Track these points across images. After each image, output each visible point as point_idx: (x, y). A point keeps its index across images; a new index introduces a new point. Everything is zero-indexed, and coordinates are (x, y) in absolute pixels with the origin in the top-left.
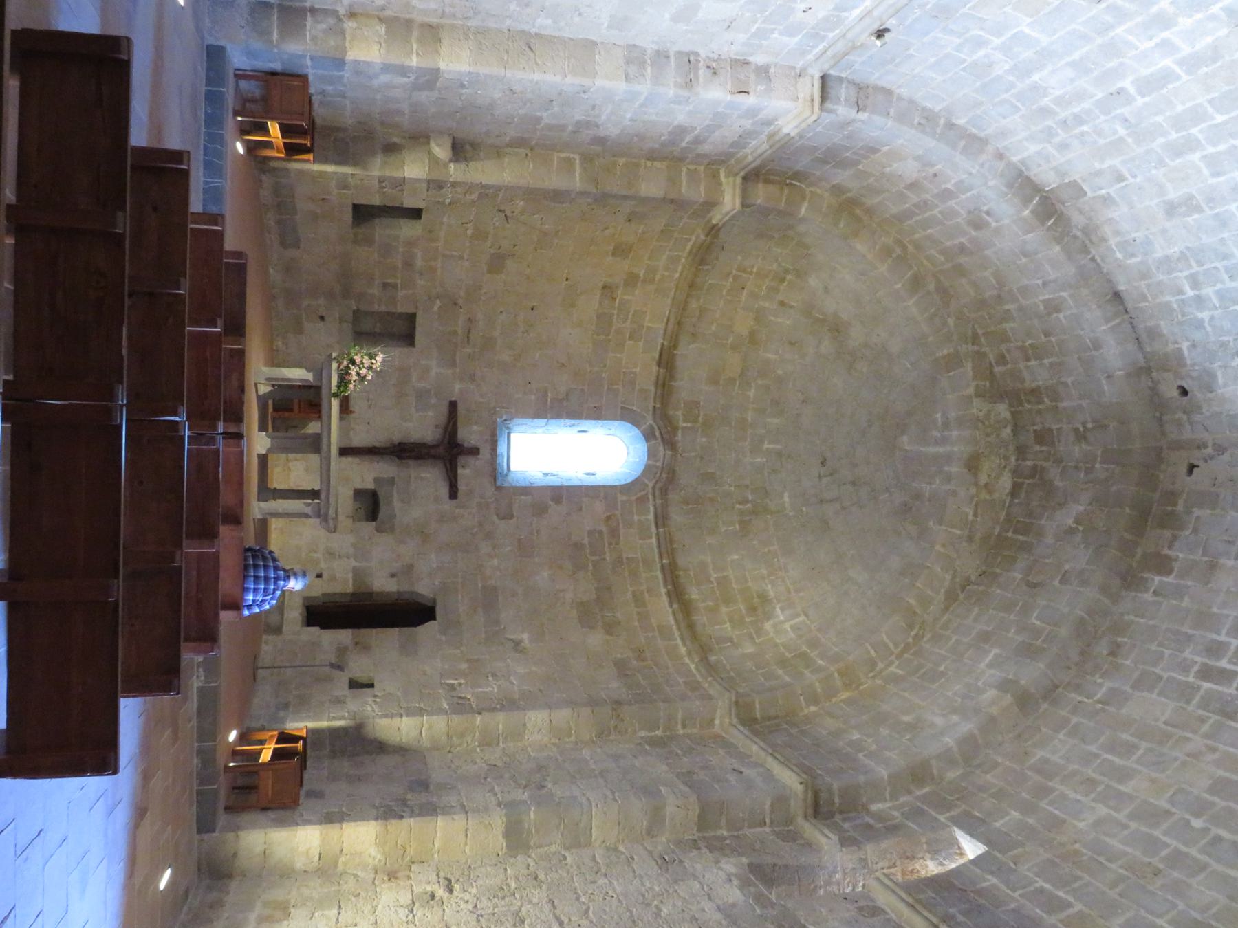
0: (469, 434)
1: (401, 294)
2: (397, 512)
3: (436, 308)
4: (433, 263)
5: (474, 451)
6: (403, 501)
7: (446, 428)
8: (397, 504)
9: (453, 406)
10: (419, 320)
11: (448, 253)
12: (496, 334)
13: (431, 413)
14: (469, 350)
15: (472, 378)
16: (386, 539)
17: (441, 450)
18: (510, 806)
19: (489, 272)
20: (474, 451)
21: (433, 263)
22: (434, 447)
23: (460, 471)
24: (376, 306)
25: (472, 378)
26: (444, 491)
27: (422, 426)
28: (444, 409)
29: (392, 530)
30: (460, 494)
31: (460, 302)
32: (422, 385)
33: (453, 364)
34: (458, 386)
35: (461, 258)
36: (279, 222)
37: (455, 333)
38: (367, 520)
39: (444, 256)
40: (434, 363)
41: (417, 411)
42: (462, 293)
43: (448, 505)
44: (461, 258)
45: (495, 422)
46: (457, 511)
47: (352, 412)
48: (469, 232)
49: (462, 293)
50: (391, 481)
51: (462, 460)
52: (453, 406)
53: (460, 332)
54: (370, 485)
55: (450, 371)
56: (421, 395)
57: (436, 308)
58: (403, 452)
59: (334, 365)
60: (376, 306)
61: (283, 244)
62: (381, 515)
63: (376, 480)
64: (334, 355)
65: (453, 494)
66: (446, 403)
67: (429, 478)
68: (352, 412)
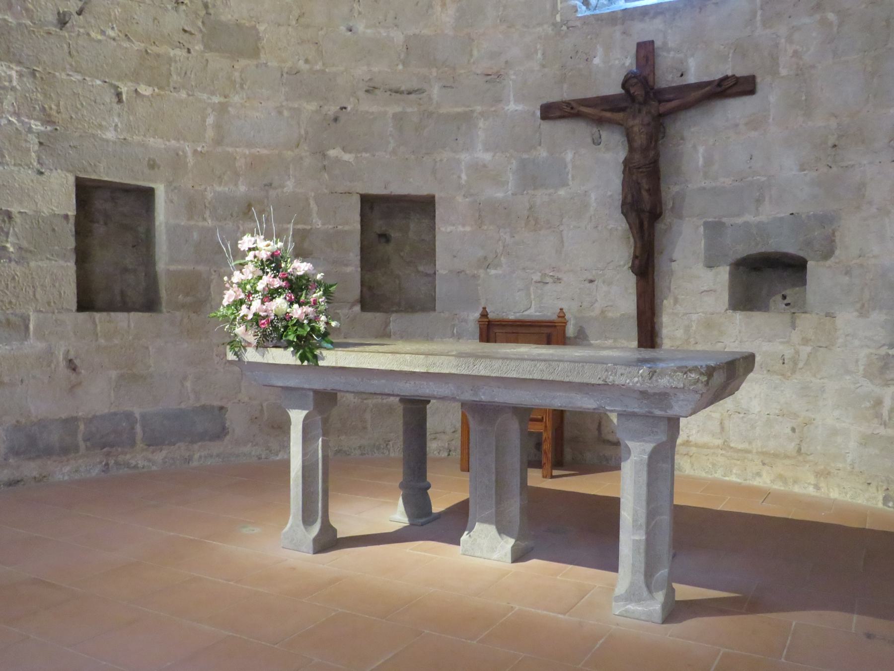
0: (607, 70)
1: (318, 223)
2: (784, 213)
3: (347, 157)
4: (240, 163)
5: (646, 52)
6: (759, 201)
7: (600, 121)
8: (767, 213)
9: (550, 112)
10: (376, 189)
11: (210, 133)
12: (398, 37)
13: (569, 156)
14: (435, 91)
15: (494, 78)
16: (852, 236)
17: (637, 124)
18: (839, 486)
19: (255, 53)
20: (646, 52)
21: (240, 163)
22: (630, 140)
23: (692, 78)
24: (349, 269)
25: (494, 78)
26: (736, 109)
27: (595, 167)
28: (561, 128)
29: (826, 220)
30: (741, 71)
31: (332, 109)
32: (511, 179)
33: (467, 118)
34: (512, 107)
35: (222, 109)
36: (154, 441)
37: (398, 118)
38: (803, 282)
39: (219, 141)
40: (465, 157)
41: (564, 184)
42: (312, 106)
43: (770, 96)
44: (222, 109)
45: (585, 20)
46: (784, 72)
47: (562, 314)
48: (145, 90)
49: (312, 106)
50: (715, 229)
51: (666, 79)
52: (550, 112)
53: (395, 109)
54: (723, 274)
55: (481, 124)
56: (531, 177)
57: (347, 157)
58: (646, 209)
59: (251, 355)
60: (349, 269)
61: (221, 433)
62: (790, 247)
63: (710, 265)
64: (231, 356)
65: (738, 87)
66: (546, 126)
67: (706, 149)
68: (562, 314)
